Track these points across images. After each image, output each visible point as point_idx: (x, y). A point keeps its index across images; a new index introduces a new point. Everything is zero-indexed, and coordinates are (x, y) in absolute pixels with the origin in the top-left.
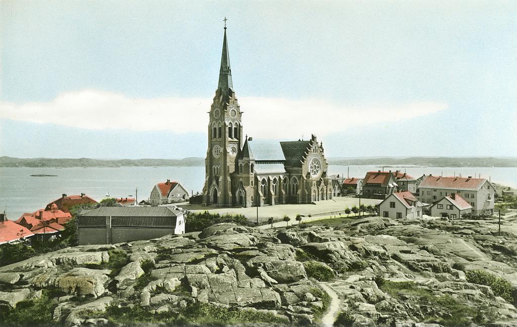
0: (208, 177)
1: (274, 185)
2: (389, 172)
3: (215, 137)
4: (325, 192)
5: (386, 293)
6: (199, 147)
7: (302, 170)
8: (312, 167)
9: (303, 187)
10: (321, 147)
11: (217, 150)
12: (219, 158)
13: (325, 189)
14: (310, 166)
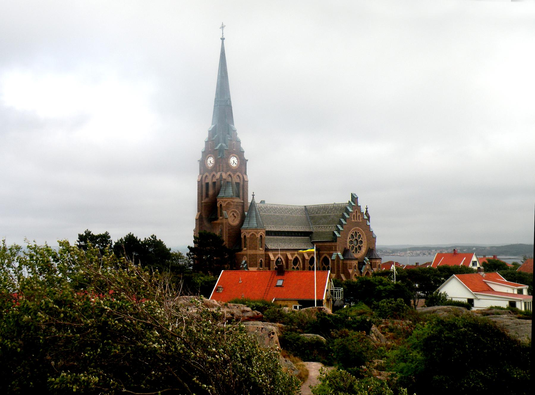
7: (336, 246)
8: (351, 242)
9: (338, 271)
14: (348, 240)
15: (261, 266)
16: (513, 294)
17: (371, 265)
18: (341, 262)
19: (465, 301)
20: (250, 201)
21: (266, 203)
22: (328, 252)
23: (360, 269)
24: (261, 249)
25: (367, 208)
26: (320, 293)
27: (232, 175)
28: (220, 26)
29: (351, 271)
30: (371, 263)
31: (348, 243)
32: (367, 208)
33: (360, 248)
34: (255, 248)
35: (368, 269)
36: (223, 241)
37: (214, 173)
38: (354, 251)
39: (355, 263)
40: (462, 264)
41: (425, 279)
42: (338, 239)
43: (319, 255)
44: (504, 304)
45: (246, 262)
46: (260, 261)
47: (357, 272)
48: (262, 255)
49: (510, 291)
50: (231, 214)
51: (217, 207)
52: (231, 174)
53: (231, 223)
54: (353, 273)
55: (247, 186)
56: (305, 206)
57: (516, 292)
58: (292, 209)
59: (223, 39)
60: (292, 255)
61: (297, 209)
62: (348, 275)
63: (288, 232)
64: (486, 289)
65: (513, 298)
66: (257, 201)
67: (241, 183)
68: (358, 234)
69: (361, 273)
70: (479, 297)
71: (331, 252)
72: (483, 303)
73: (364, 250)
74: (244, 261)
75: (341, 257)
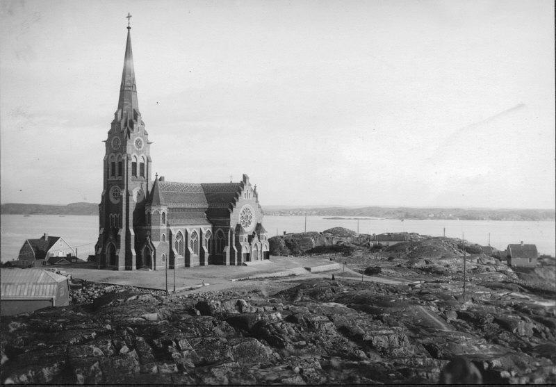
0: (103, 229)
4: (259, 250)
6: (90, 184)
9: (231, 243)
13: (259, 246)
14: (240, 216)
27: (137, 156)
29: (242, 243)
67: (146, 164)
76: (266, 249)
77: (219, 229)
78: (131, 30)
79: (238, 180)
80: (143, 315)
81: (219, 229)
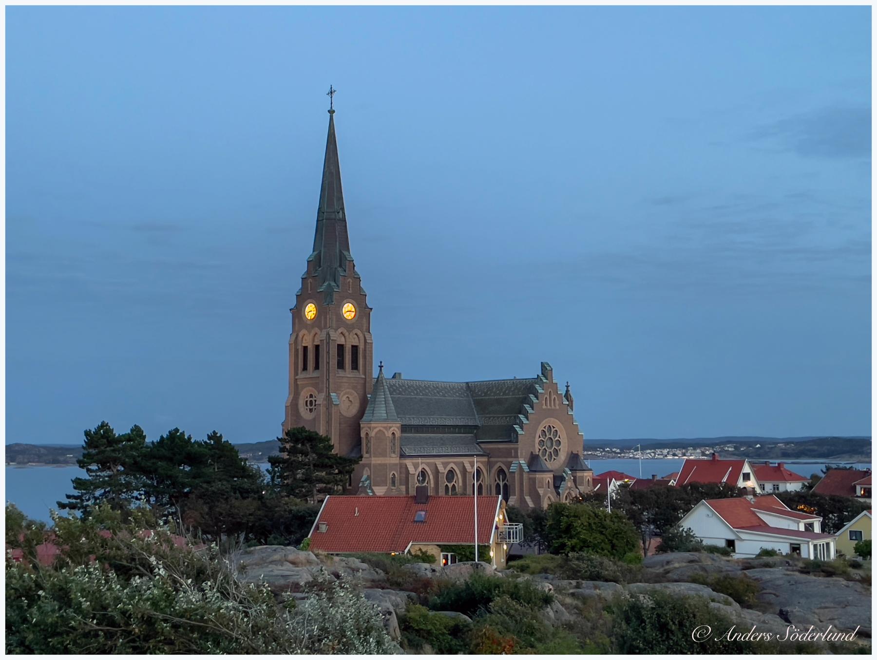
1: (450, 485)
2: (651, 478)
3: (305, 368)
5: (647, 602)
7: (516, 450)
8: (542, 443)
9: (521, 490)
10: (567, 396)
11: (309, 399)
12: (314, 419)
14: (537, 440)
15: (393, 483)
16: (797, 533)
17: (575, 481)
18: (525, 476)
19: (722, 544)
20: (375, 374)
21: (403, 377)
22: (504, 460)
23: (557, 487)
24: (393, 455)
25: (567, 387)
26: (485, 535)
27: (347, 334)
28: (328, 90)
29: (541, 491)
30: (575, 477)
31: (537, 445)
32: (567, 387)
33: (556, 452)
34: (384, 455)
35: (570, 488)
36: (331, 447)
37: (317, 330)
38: (546, 457)
39: (548, 477)
40: (725, 480)
41: (659, 507)
42: (520, 438)
43: (490, 465)
44: (783, 548)
45: (369, 478)
46: (391, 476)
47: (551, 493)
48: (396, 465)
49: (793, 526)
50: (344, 398)
51: (360, 438)
52: (345, 331)
53: (345, 414)
54: (545, 495)
55: (371, 352)
56: (467, 383)
57: (802, 528)
58: (446, 388)
59: (331, 112)
60: (445, 465)
61: (454, 388)
62: (537, 498)
63: (438, 426)
64: (756, 523)
65: (795, 540)
66: (387, 374)
67: (361, 347)
68: (553, 430)
69: (558, 494)
70: (743, 536)
71: (510, 460)
72: (749, 545)
73: (563, 456)
74: (365, 477)
75: (526, 468)
76: (303, 502)
77: (499, 464)
78: (334, 95)
79: (533, 372)
80: (270, 559)
81: (499, 464)
